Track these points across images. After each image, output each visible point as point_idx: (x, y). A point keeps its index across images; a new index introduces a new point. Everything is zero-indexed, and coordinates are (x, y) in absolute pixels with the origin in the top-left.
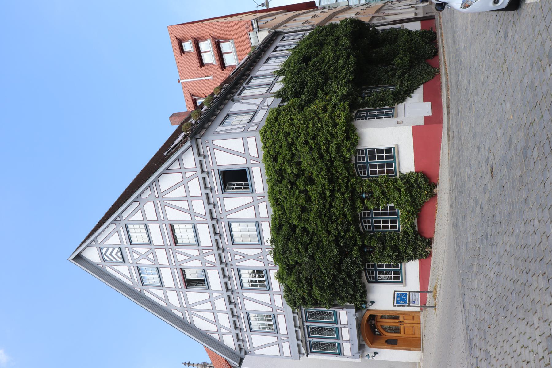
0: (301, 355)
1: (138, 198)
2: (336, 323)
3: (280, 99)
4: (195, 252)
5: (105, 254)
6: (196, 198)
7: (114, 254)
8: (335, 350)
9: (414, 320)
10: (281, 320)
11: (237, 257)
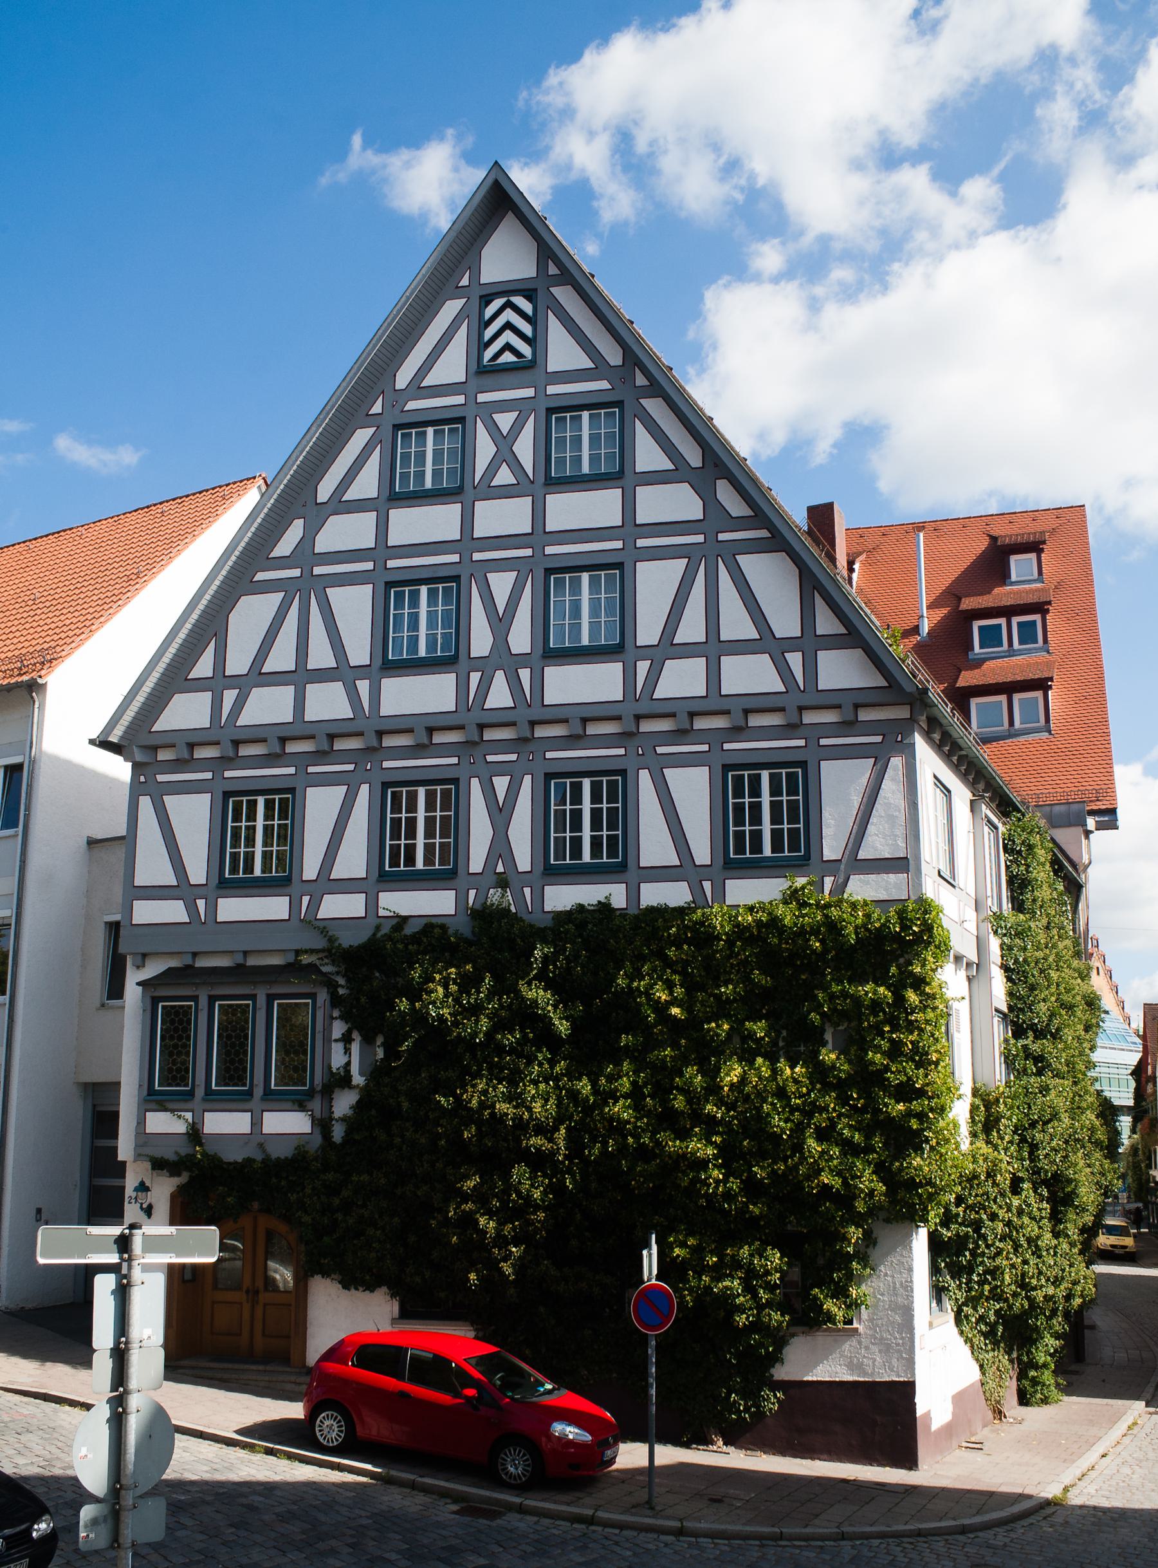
0: (140, 957)
1: (716, 465)
2: (268, 1093)
3: (1005, 1010)
4: (521, 639)
5: (509, 305)
6: (714, 676)
7: (508, 337)
8: (280, 1081)
9: (264, 1335)
10: (275, 907)
11: (501, 784)
